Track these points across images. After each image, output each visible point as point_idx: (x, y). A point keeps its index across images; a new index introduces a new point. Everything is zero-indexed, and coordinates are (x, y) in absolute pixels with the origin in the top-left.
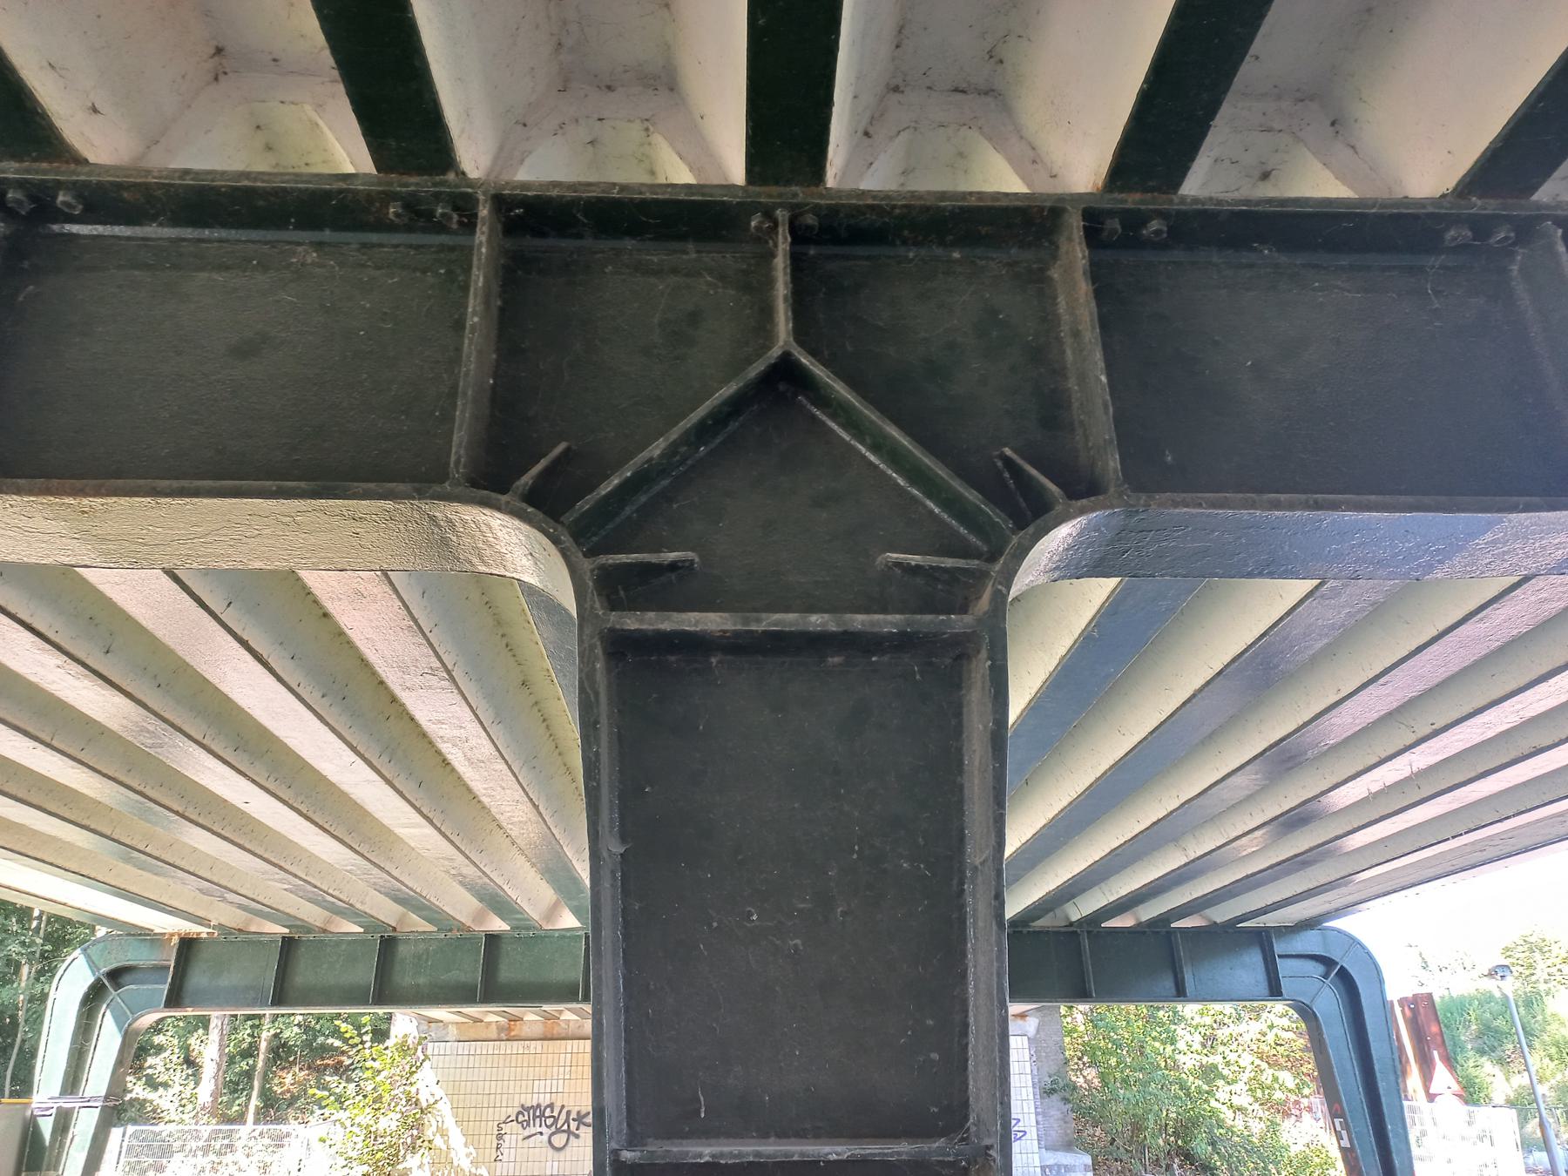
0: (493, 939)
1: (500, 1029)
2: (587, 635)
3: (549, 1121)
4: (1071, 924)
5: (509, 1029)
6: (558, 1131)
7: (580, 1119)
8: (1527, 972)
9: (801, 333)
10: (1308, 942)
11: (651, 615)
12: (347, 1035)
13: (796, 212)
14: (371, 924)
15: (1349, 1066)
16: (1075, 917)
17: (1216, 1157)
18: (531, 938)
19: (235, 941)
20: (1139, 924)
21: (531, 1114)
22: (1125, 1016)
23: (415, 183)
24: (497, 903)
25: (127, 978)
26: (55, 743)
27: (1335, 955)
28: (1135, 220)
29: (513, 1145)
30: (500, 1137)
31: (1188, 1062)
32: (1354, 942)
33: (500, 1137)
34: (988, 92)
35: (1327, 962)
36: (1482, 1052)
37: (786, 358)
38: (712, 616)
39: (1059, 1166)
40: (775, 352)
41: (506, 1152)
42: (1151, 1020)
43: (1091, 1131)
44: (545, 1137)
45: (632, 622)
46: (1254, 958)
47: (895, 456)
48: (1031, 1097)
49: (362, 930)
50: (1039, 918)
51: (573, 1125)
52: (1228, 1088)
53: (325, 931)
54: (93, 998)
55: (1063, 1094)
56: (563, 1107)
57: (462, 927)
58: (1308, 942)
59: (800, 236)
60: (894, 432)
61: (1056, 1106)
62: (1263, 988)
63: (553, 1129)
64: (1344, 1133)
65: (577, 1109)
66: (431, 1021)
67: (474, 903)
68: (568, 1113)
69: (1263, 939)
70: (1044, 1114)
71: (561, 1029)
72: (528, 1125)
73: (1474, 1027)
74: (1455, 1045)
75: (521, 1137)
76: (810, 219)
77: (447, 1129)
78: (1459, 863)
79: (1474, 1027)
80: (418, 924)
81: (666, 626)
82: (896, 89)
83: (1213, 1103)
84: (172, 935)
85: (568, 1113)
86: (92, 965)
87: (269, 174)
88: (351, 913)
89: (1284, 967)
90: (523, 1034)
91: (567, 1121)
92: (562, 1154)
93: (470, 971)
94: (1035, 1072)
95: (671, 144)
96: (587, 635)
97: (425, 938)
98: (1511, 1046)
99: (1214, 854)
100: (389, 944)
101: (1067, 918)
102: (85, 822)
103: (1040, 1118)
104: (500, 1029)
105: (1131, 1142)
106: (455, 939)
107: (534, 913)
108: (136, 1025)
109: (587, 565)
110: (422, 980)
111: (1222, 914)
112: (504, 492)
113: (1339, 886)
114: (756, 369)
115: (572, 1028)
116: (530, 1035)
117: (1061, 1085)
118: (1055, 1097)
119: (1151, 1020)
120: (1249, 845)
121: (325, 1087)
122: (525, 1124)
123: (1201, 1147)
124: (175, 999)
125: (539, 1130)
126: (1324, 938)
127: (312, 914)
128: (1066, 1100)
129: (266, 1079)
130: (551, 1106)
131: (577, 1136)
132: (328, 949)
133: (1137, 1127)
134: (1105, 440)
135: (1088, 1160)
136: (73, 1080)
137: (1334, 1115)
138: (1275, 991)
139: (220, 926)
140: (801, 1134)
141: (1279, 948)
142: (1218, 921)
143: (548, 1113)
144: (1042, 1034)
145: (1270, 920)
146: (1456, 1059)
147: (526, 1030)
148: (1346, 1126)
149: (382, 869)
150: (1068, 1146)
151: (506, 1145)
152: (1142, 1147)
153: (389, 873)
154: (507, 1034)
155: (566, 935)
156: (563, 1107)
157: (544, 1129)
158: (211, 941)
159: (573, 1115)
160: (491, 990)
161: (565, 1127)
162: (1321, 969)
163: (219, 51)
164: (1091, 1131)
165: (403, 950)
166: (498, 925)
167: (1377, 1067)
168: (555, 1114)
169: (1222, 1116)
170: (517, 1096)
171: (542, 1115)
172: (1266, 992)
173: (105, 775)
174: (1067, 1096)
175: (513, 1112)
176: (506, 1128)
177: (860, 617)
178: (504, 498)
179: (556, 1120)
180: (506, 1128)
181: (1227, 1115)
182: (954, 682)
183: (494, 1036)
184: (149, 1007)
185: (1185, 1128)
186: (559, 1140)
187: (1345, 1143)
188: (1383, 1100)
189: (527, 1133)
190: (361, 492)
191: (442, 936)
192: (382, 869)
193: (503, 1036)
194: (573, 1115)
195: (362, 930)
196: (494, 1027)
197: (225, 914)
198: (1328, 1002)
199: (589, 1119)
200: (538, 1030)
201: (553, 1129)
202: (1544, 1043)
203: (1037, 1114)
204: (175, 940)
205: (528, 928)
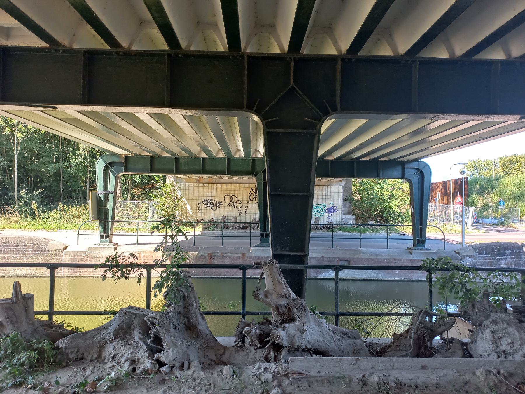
0: (203, 159)
1: (197, 180)
3: (211, 203)
4: (352, 159)
5: (199, 180)
6: (214, 206)
8: (507, 171)
9: (295, 82)
10: (415, 165)
11: (273, 129)
12: (157, 180)
13: (294, 58)
14: (173, 154)
15: (417, 194)
16: (353, 157)
17: (389, 217)
18: (214, 159)
19: (138, 157)
20: (370, 159)
22: (371, 182)
23: (234, 54)
24: (204, 149)
25: (113, 165)
26: (121, 117)
27: (420, 168)
28: (350, 60)
29: (202, 209)
30: (199, 207)
31: (386, 193)
32: (426, 165)
33: (199, 207)
34: (329, 28)
35: (418, 169)
36: (478, 193)
37: (292, 87)
38: (281, 130)
39: (346, 218)
40: (291, 86)
41: (200, 210)
42: (378, 183)
43: (357, 211)
44: (211, 207)
45: (270, 130)
46: (400, 168)
47: (308, 102)
48: (341, 201)
49: (170, 155)
50: (343, 158)
51: (218, 205)
52: (395, 201)
53: (161, 155)
54: (106, 169)
55: (350, 201)
56: (215, 200)
57: (195, 156)
58: (415, 165)
59: (295, 61)
60: (308, 100)
61: (348, 204)
62: (400, 175)
63: (213, 205)
64: (413, 209)
65: (219, 201)
66: (177, 177)
67: (199, 149)
68: (216, 202)
69: (402, 164)
70: (344, 206)
71: (213, 181)
72: (206, 204)
73: (478, 186)
74: (471, 191)
75: (204, 207)
76: (297, 59)
78: (449, 147)
79: (478, 186)
80: (184, 153)
81: (275, 131)
82: (313, 27)
83: (391, 204)
84: (122, 155)
85: (216, 202)
86: (105, 162)
87: (254, 114)
88: (169, 151)
89: (406, 171)
90: (203, 182)
91: (216, 203)
92: (215, 211)
93: (200, 167)
94: (343, 195)
95: (274, 38)
97: (186, 158)
98: (487, 192)
99: (400, 138)
100: (177, 159)
101: (352, 157)
102: (117, 131)
103: (343, 207)
105: (367, 213)
106: (194, 159)
107: (214, 153)
108: (118, 176)
109: (264, 122)
110: (187, 168)
111: (392, 157)
112: (252, 110)
113: (426, 150)
114: (288, 89)
115: (216, 181)
116: (205, 182)
117: (350, 198)
118: (348, 202)
119: (378, 183)
120: (405, 138)
121: (152, 193)
123: (385, 215)
124: (126, 170)
125: (209, 205)
126: (419, 164)
127: (158, 151)
128: (351, 203)
129: (131, 191)
130: (212, 200)
131: (219, 207)
132: (162, 160)
133: (370, 210)
135: (354, 217)
136: (106, 187)
137: (411, 205)
138: (403, 176)
139: (135, 153)
140: (292, 192)
141: (406, 166)
142: (391, 159)
143: (211, 201)
144: (346, 186)
145: (405, 159)
146: (470, 195)
147: (204, 181)
148: (413, 207)
149: (181, 143)
150: (349, 214)
151: (201, 208)
152: (370, 215)
153: (183, 144)
154: (199, 182)
155: (221, 159)
156: (215, 200)
157: (210, 205)
158: (132, 157)
159: (218, 202)
160: (204, 171)
161: (216, 205)
162: (416, 171)
163: (198, 22)
164: (357, 211)
165: (181, 161)
166: (204, 155)
167: (424, 194)
168: (213, 202)
169: (393, 207)
170: (202, 197)
172: (401, 176)
173: (129, 123)
174: (351, 201)
176: (200, 205)
177: (301, 130)
178: (252, 111)
179: (213, 203)
180: (200, 205)
181: (395, 208)
182: (313, 138)
183: (195, 182)
184: (120, 172)
185: (382, 211)
186: (214, 208)
187: (413, 211)
188: (424, 202)
189: (206, 206)
191: (191, 157)
192: (181, 143)
193: (197, 182)
194: (218, 202)
195: (170, 155)
196: (195, 179)
197: (137, 151)
198: (416, 179)
200: (207, 181)
201: (213, 205)
202: (497, 191)
203: (342, 205)
204: (123, 156)
205: (213, 157)
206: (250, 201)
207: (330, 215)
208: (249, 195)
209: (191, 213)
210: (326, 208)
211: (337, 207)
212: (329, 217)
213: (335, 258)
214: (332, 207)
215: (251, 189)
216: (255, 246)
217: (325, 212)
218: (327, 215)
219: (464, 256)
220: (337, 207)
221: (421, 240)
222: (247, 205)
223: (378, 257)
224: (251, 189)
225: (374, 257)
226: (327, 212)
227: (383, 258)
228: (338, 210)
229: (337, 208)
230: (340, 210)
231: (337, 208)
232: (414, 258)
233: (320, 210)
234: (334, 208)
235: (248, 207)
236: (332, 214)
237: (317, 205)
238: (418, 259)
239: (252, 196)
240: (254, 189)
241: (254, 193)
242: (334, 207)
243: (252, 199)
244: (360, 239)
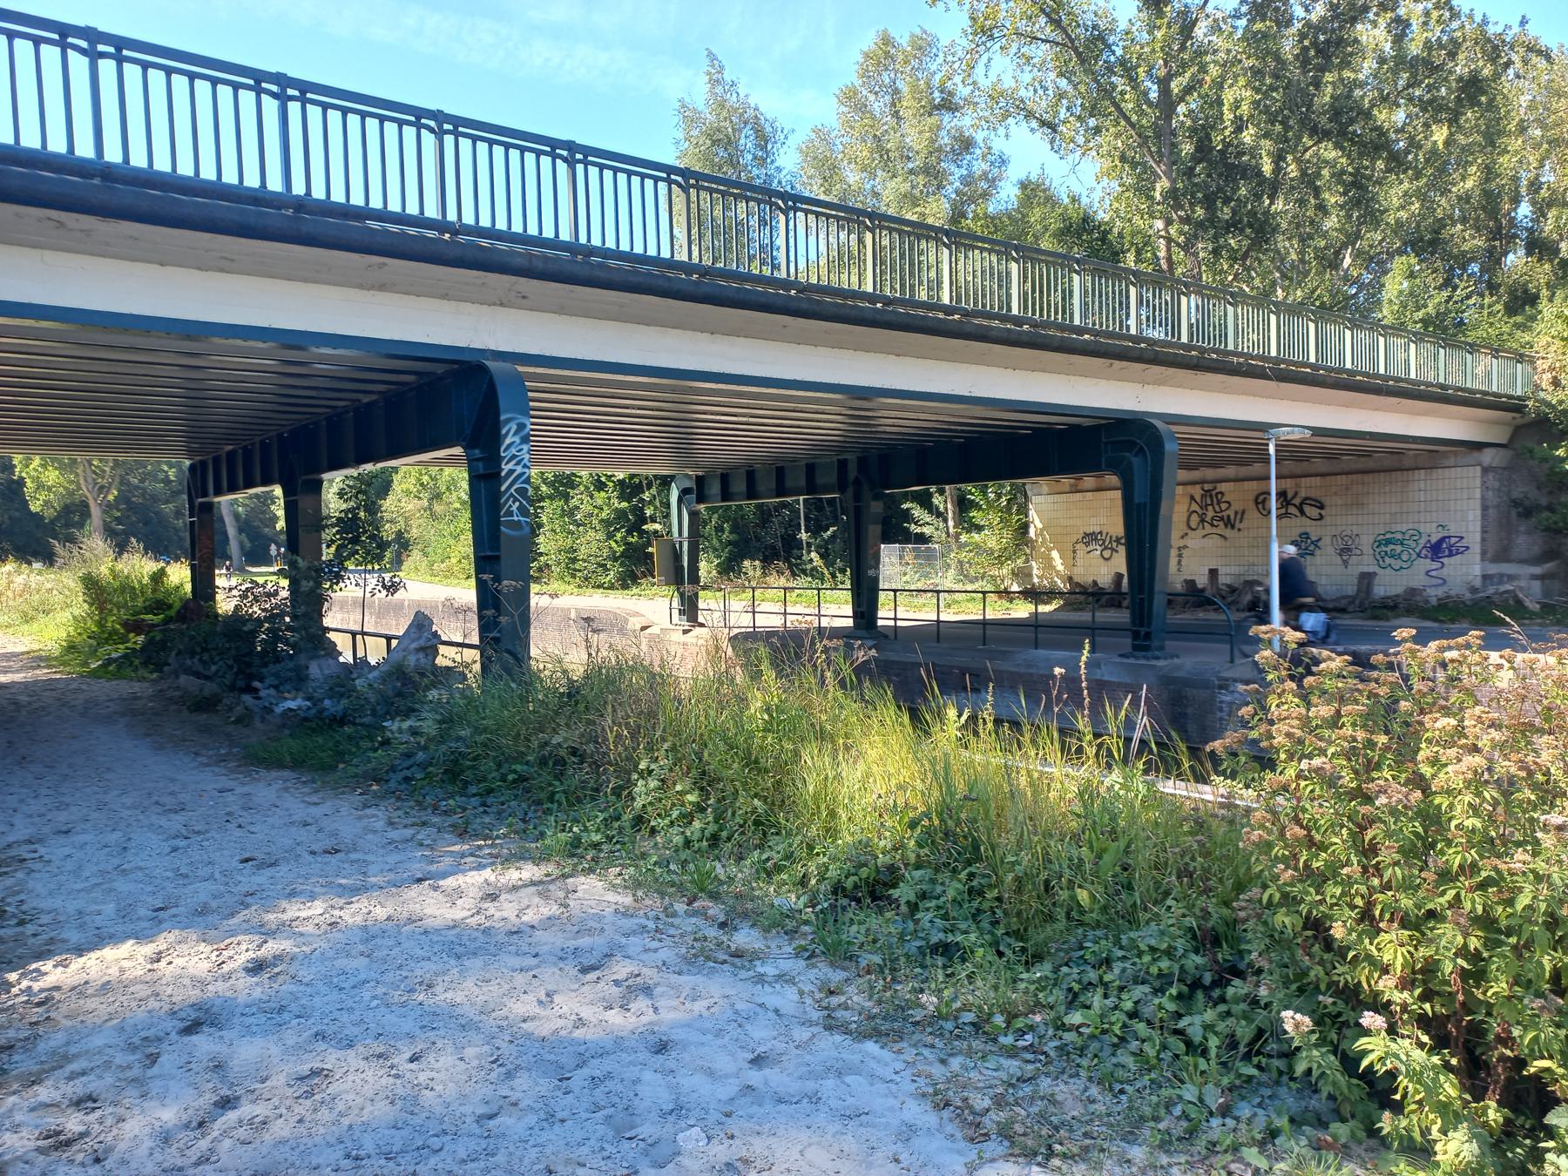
1: (1071, 485)
2: (158, 577)
6: (1106, 548)
7: (1118, 540)
21: (1090, 538)
30: (1074, 552)
51: (1114, 544)
77: (1098, 1166)
96: (158, 577)
104: (1071, 485)
122: (1087, 544)
130: (1101, 533)
134: (1453, 121)
154: (1075, 490)
171: (1096, 539)
175: (1080, 537)
176: (1078, 546)
179: (1104, 541)
186: (1107, 554)
190: (1341, 984)
199: (1123, 541)
204: (743, 471)
206: (1189, 532)
207: (1436, 565)
208: (1186, 515)
209: (1060, 568)
210: (1423, 541)
211: (1462, 538)
212: (1433, 573)
213: (953, 667)
214: (1445, 538)
215: (1192, 498)
216: (1120, 656)
217: (1419, 555)
218: (1427, 564)
219: (1227, 680)
220: (1462, 538)
221: (1143, 630)
222: (1182, 543)
223: (1031, 671)
224: (1192, 498)
225: (1023, 670)
226: (1426, 557)
227: (1042, 672)
228: (1468, 548)
229: (1464, 543)
230: (1476, 549)
231: (1464, 543)
232: (1106, 678)
233: (1399, 548)
234: (1453, 540)
235: (1185, 547)
236: (1445, 560)
237: (1388, 536)
238: (1113, 679)
239: (1195, 519)
240: (1198, 499)
241: (1198, 509)
242: (1449, 537)
243: (1193, 525)
244: (785, 614)
